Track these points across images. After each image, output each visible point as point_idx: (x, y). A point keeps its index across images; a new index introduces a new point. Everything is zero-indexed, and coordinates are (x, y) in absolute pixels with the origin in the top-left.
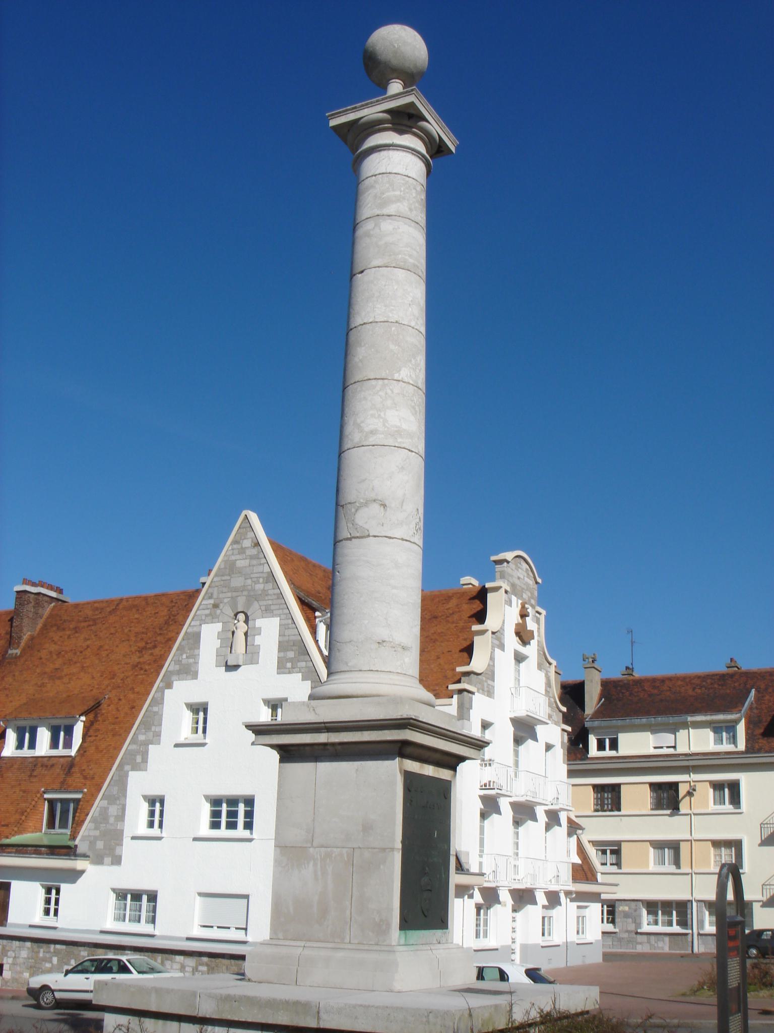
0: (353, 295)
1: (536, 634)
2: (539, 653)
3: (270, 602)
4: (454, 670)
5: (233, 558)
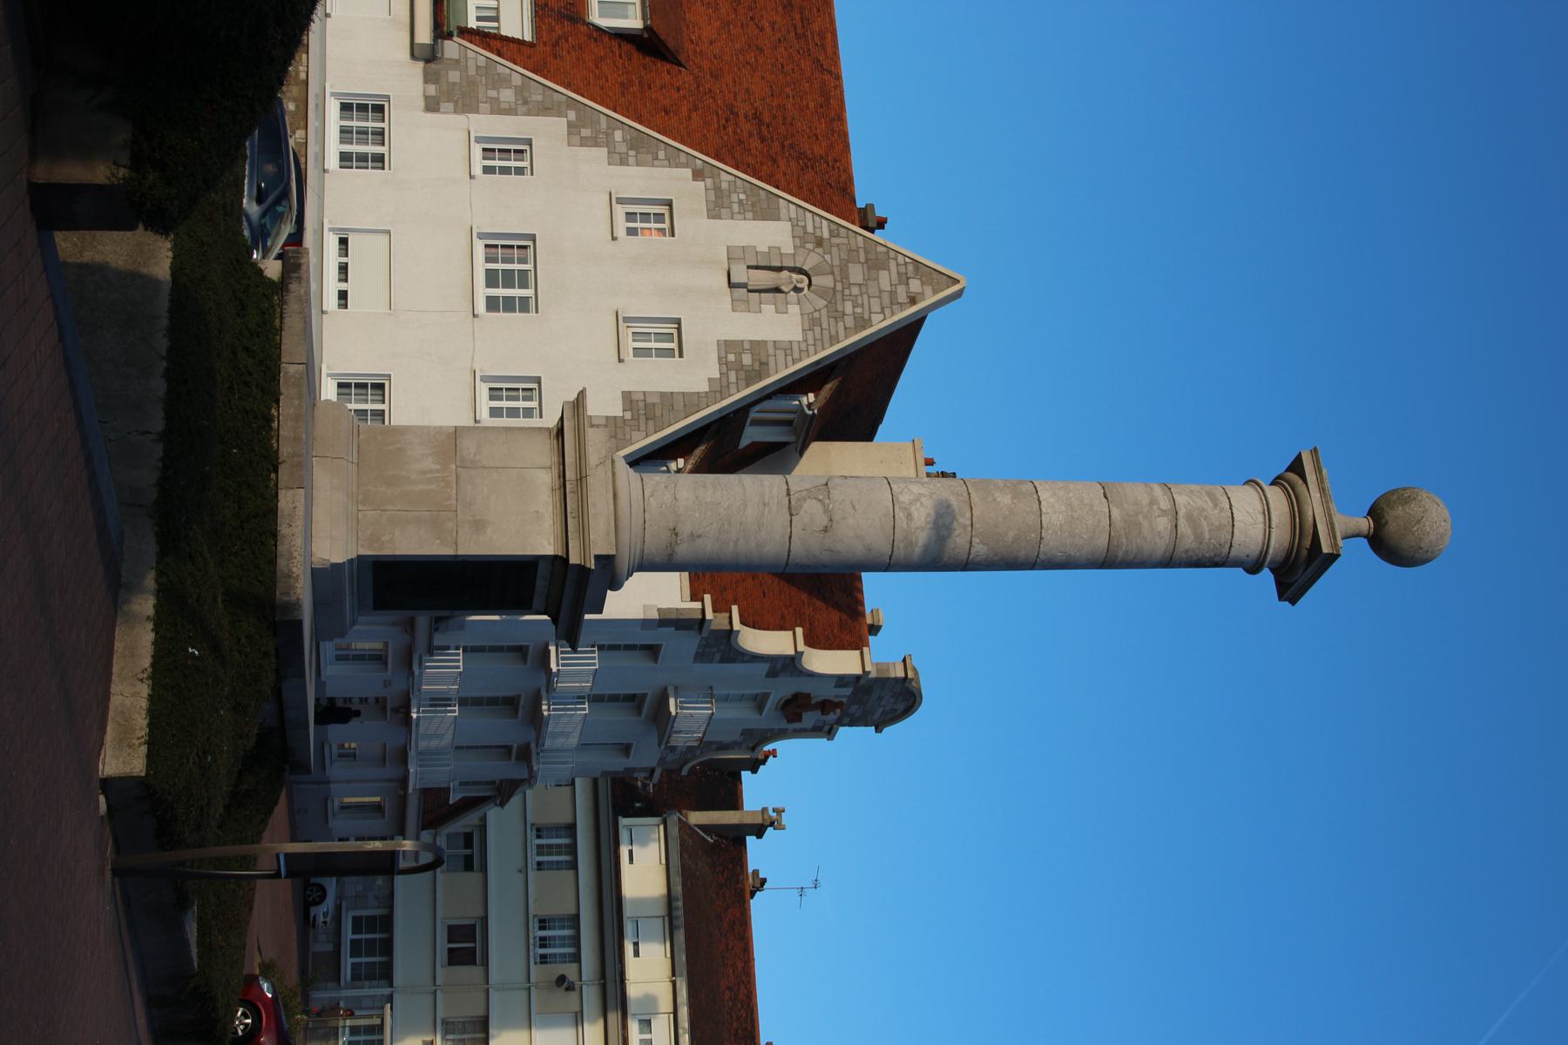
0: (673, 616)
1: (797, 725)
3: (825, 325)
5: (893, 264)
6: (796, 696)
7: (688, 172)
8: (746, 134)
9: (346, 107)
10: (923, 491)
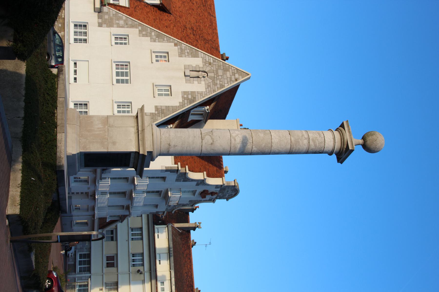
1: (204, 199)
3: (212, 87)
4: (187, 165)
5: (230, 70)
6: (204, 191)
7: (173, 44)
8: (189, 33)
9: (76, 26)
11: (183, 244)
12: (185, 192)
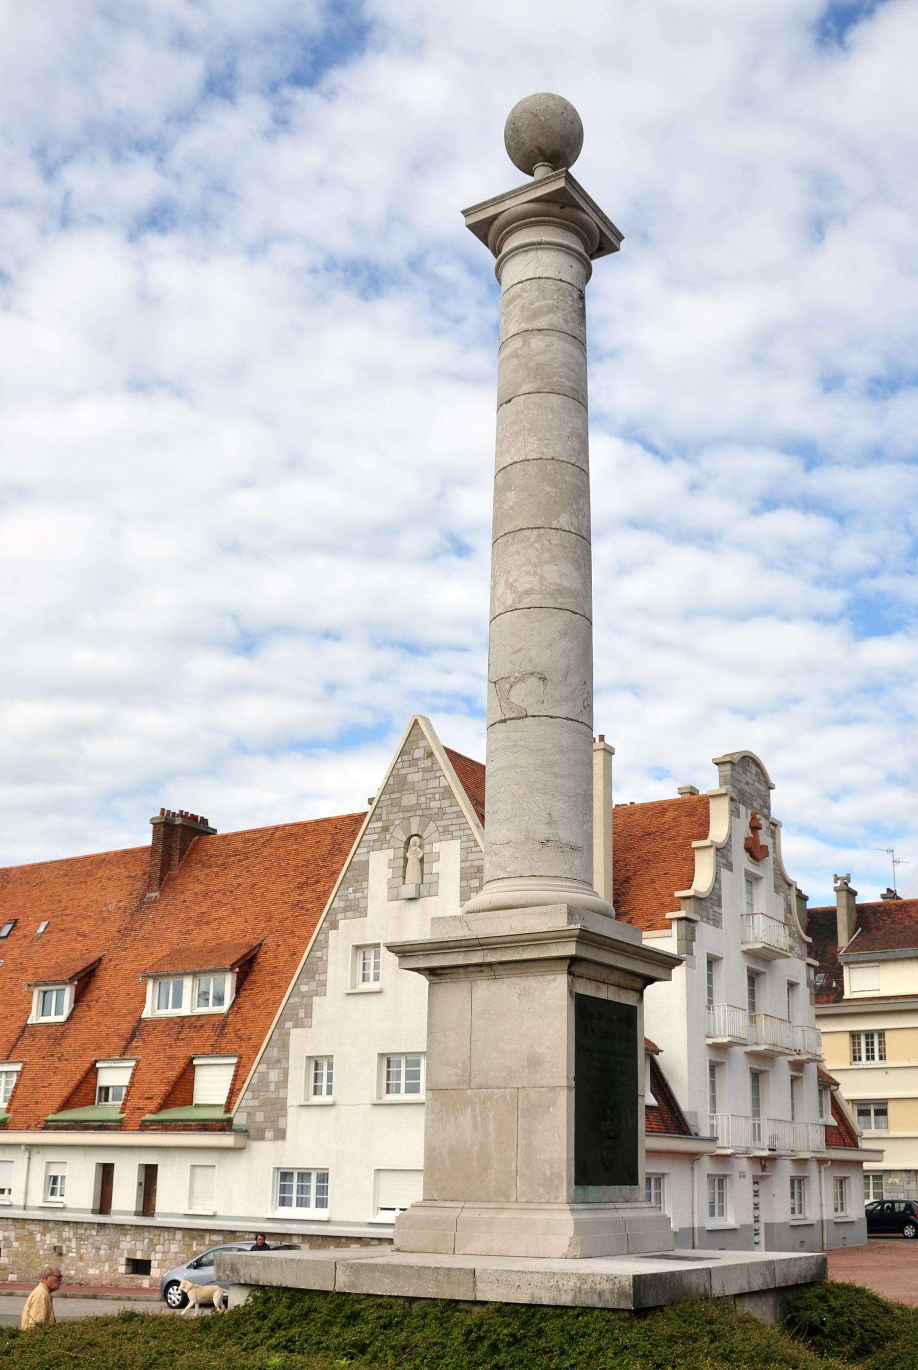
1: (771, 850)
2: (775, 874)
3: (449, 822)
4: (672, 895)
5: (403, 772)
6: (748, 849)
7: (332, 933)
8: (313, 894)
9: (284, 1202)
10: (503, 582)
11: (893, 922)
12: (750, 904)
